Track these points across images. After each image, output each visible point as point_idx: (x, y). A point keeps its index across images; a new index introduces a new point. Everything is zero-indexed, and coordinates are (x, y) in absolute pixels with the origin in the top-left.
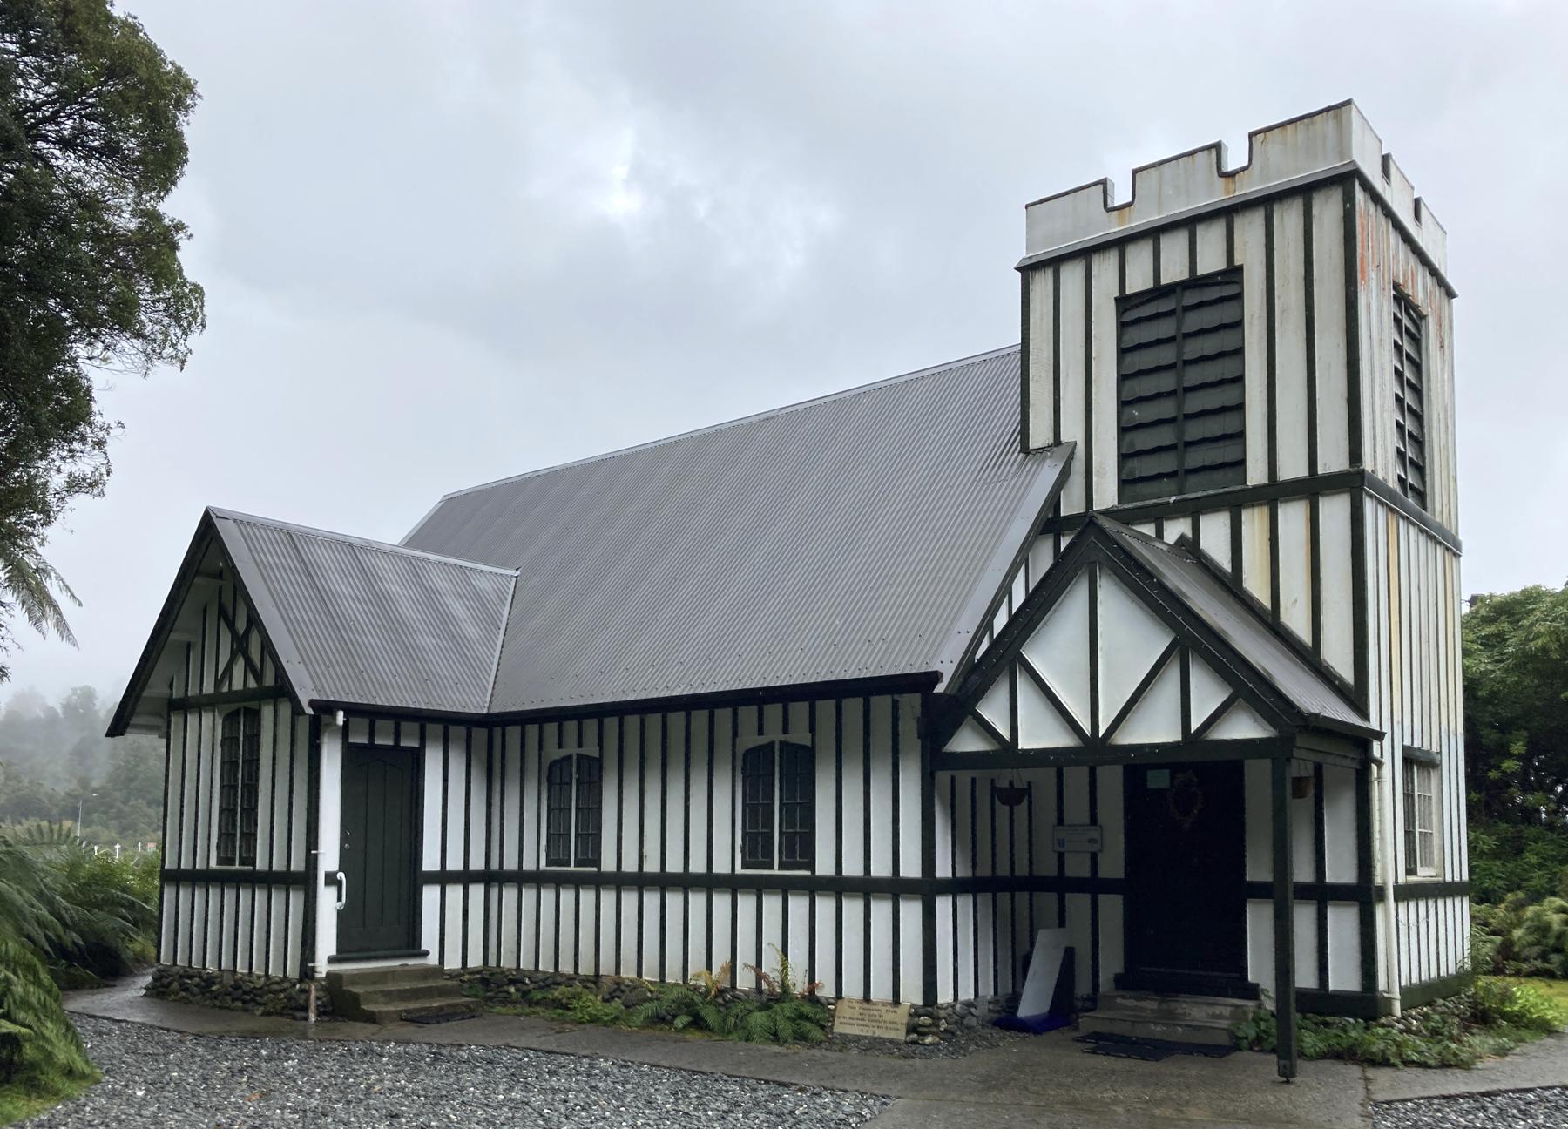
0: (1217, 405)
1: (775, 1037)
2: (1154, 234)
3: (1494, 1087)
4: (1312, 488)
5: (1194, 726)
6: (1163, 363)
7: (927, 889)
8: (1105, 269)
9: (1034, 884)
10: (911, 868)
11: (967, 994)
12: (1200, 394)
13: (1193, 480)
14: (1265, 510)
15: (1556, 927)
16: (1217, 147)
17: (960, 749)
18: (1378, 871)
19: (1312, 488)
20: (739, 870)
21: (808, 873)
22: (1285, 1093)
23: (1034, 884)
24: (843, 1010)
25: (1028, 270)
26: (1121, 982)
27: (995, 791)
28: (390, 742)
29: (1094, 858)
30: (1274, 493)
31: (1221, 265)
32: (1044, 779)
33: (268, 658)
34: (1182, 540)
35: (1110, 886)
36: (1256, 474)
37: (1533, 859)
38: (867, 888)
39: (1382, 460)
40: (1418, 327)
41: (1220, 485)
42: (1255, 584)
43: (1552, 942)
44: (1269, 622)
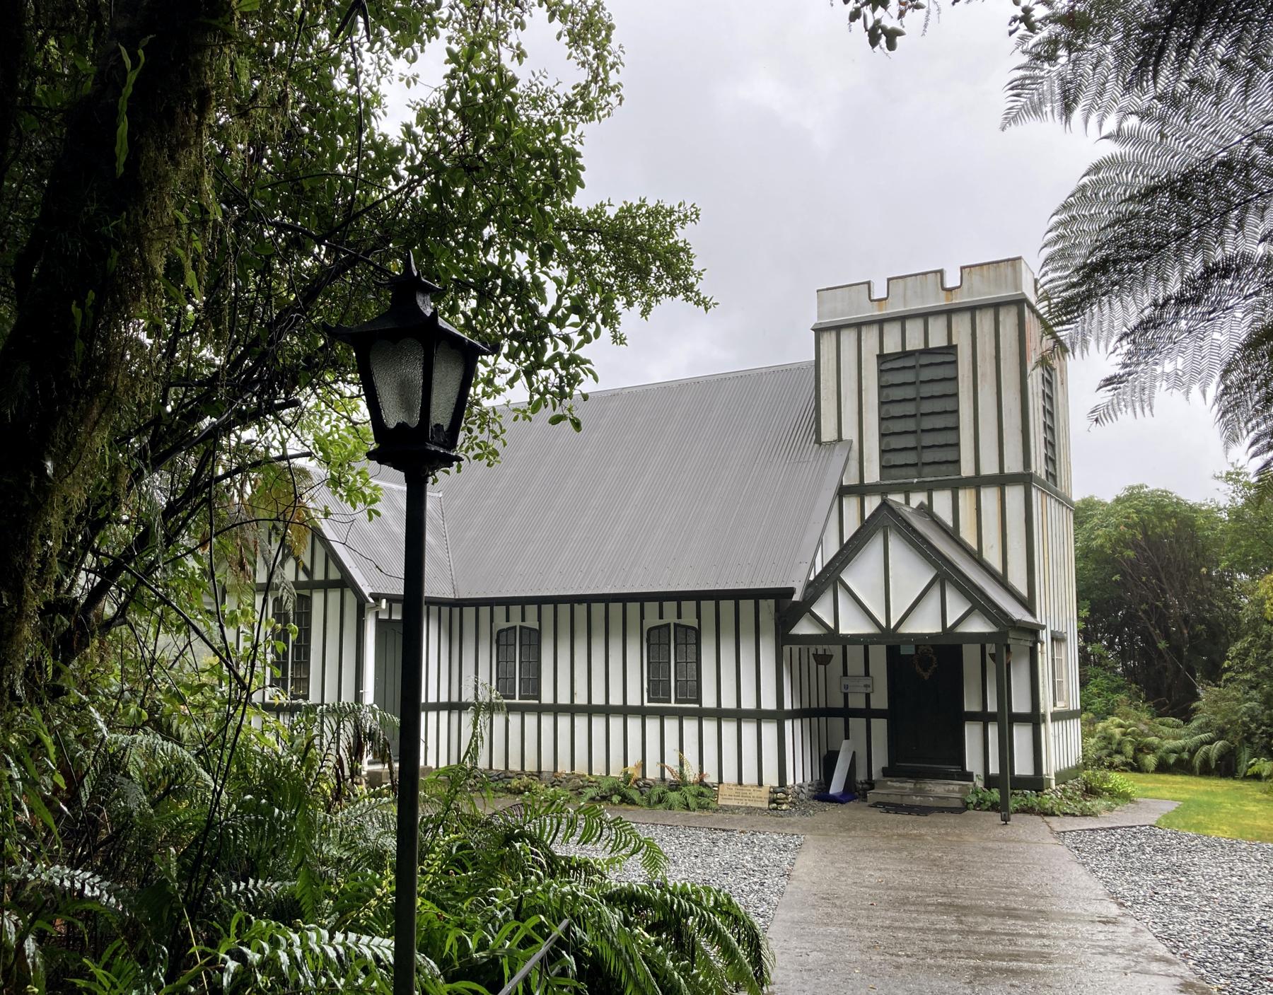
0: (943, 426)
1: (687, 807)
2: (902, 319)
3: (1114, 825)
4: (1001, 481)
5: (949, 625)
6: (908, 397)
7: (779, 716)
8: (870, 338)
9: (829, 712)
10: (769, 703)
11: (799, 781)
12: (932, 418)
13: (927, 470)
14: (973, 492)
15: (1118, 737)
16: (941, 272)
17: (801, 633)
18: (1042, 705)
19: (1001, 481)
20: (646, 704)
21: (697, 706)
22: (1008, 828)
23: (829, 712)
24: (723, 790)
25: (819, 331)
26: (886, 772)
27: (816, 656)
28: (387, 617)
29: (868, 696)
30: (978, 482)
31: (944, 343)
32: (855, 653)
33: (331, 563)
34: (921, 506)
35: (879, 714)
36: (967, 470)
37: (1095, 690)
38: (739, 715)
39: (1039, 467)
40: (1051, 376)
41: (943, 474)
42: (968, 535)
43: (1114, 747)
44: (976, 558)
